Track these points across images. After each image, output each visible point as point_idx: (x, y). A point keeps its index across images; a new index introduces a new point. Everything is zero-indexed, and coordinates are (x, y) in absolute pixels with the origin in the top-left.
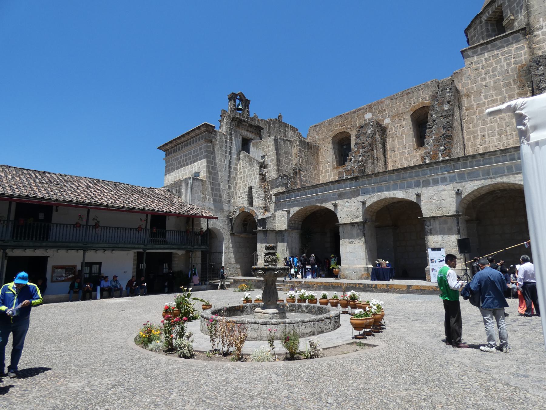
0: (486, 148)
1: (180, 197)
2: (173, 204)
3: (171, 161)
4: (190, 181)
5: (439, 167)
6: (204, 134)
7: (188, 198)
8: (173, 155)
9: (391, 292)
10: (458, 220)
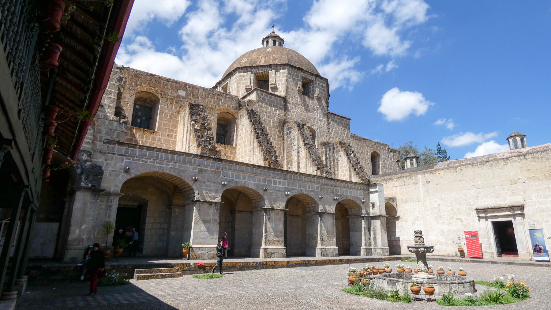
0: (242, 161)
5: (278, 173)
9: (276, 268)
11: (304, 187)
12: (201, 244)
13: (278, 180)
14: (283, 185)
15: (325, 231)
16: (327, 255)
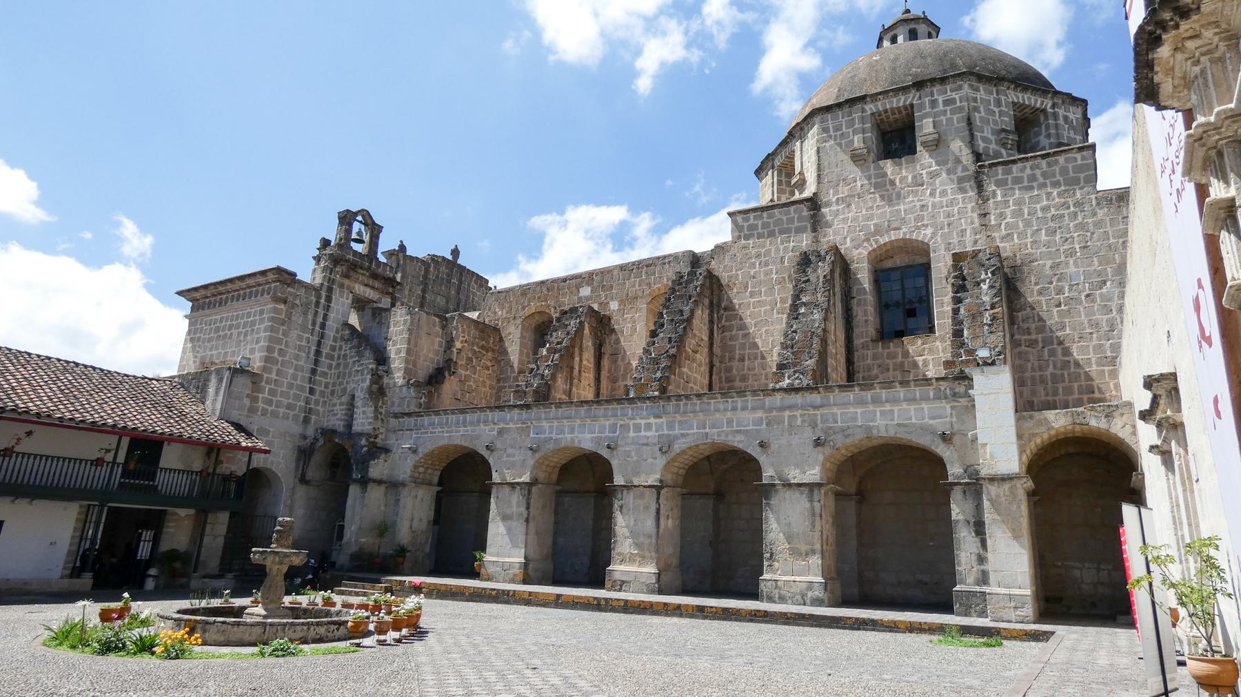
1: (203, 403)
2: (182, 415)
3: (201, 324)
4: (227, 375)
5: (645, 405)
6: (273, 285)
7: (218, 406)
8: (207, 311)
10: (659, 494)
11: (713, 426)
12: (498, 555)
13: (643, 422)
14: (657, 431)
15: (781, 534)
16: (782, 599)
